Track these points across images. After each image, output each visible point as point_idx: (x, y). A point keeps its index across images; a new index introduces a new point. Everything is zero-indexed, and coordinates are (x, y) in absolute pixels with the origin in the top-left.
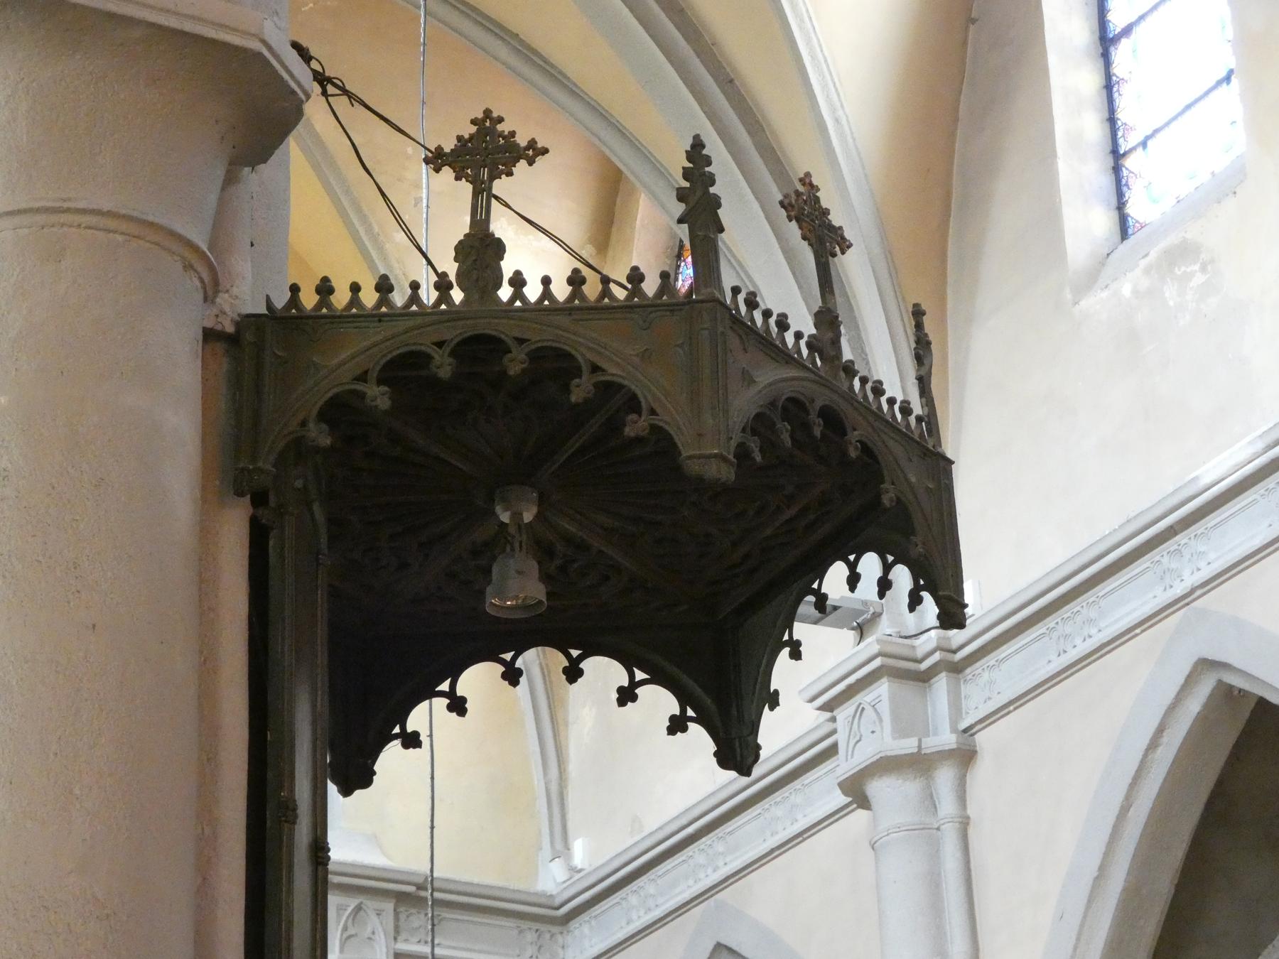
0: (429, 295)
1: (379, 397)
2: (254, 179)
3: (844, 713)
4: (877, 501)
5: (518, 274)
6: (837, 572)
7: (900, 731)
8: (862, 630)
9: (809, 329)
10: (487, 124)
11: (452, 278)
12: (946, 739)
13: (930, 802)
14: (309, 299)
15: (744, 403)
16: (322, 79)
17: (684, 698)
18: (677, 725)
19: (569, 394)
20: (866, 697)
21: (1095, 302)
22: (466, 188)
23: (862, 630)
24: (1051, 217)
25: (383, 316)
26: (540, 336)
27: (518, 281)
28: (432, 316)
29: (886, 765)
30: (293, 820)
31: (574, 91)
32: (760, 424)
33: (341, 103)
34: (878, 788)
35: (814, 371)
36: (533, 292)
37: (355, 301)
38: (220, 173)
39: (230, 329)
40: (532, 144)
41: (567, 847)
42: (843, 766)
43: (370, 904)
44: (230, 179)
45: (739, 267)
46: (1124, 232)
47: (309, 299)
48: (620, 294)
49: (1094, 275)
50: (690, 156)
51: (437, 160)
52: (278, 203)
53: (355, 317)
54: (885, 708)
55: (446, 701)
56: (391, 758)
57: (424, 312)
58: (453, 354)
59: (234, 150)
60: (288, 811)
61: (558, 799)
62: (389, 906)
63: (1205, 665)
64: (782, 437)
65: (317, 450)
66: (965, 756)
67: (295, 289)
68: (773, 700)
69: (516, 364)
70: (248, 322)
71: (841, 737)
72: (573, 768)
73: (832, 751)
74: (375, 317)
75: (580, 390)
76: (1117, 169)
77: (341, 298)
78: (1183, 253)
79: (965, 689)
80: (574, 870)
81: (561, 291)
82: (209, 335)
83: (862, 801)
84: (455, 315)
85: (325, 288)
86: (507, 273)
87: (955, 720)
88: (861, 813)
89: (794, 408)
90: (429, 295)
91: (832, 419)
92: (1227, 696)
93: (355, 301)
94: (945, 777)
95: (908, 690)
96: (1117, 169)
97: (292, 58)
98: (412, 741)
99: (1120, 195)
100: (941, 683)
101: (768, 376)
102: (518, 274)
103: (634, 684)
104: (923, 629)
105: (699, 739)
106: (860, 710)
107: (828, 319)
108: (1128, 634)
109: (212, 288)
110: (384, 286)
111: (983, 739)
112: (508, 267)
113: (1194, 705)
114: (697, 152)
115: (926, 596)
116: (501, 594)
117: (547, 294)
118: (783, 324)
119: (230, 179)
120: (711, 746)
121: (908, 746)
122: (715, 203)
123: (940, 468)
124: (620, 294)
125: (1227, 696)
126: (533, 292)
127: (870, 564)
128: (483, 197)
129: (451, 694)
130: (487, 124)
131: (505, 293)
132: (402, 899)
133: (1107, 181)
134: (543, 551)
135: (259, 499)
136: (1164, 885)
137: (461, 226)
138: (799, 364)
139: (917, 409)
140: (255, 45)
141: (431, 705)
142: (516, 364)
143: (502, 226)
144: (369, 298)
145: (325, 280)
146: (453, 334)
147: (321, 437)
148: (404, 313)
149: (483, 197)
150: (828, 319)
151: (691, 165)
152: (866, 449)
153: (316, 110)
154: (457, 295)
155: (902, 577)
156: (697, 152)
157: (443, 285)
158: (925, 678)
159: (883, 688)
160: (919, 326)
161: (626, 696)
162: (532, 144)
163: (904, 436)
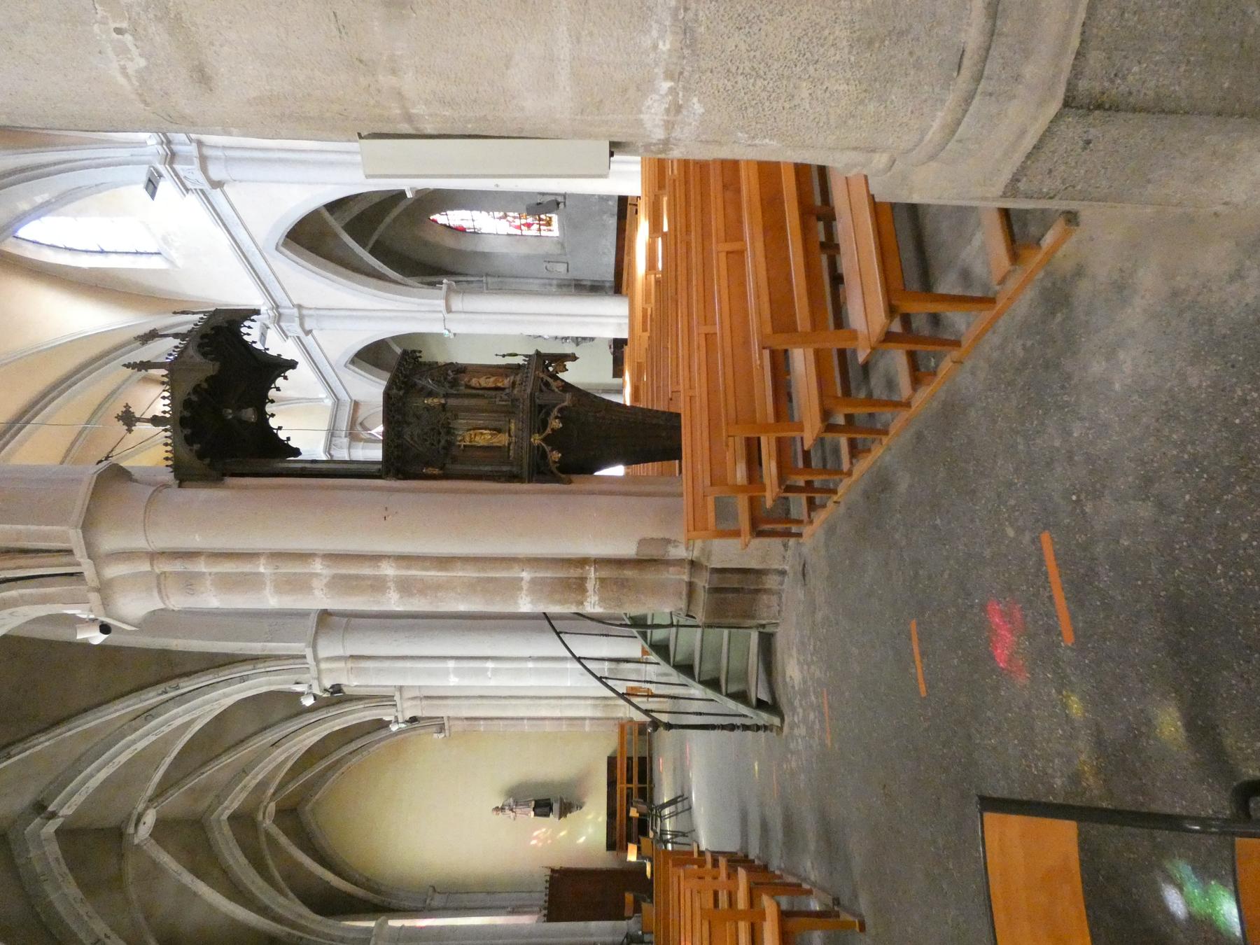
0: (168, 434)
1: (196, 447)
2: (136, 475)
3: (289, 334)
4: (227, 327)
6: (246, 338)
7: (293, 321)
8: (268, 328)
9: (179, 341)
10: (119, 418)
12: (295, 311)
13: (310, 316)
14: (170, 463)
15: (198, 358)
16: (107, 458)
17: (279, 376)
18: (286, 378)
19: (642, 125)
20: (285, 328)
21: (179, 263)
22: (137, 424)
23: (268, 328)
24: (154, 271)
25: (174, 445)
27: (164, 412)
28: (175, 432)
29: (302, 325)
30: (306, 468)
31: (118, 388)
32: (204, 355)
33: (114, 453)
34: (307, 327)
35: (190, 340)
36: (168, 409)
37: (170, 452)
38: (135, 484)
39: (178, 482)
40: (125, 407)
41: (321, 399)
42: (302, 335)
43: (333, 443)
44: (136, 481)
45: (158, 356)
46: (159, 253)
47: (170, 463)
48: (168, 387)
49: (172, 262)
50: (128, 368)
51: (130, 431)
52: (146, 469)
53: (174, 452)
54: (288, 324)
56: (292, 444)
60: (302, 469)
61: (310, 400)
62: (334, 439)
63: (277, 249)
65: (211, 461)
66: (300, 307)
67: (167, 466)
68: (279, 355)
69: (187, 414)
70: (176, 477)
71: (295, 335)
72: (302, 396)
73: (298, 338)
74: (174, 447)
75: (194, 398)
76: (142, 253)
77: (170, 455)
78: (165, 239)
79: (283, 305)
80: (327, 397)
81: (167, 402)
82: (180, 486)
83: (310, 332)
84: (173, 426)
85: (167, 459)
86: (163, 415)
87: (289, 308)
88: (314, 332)
89: (200, 346)
90: (168, 434)
91: (203, 337)
92: (285, 244)
93: (170, 452)
94: (305, 312)
95: (283, 318)
96: (142, 253)
97: (101, 465)
98: (288, 439)
99: (148, 253)
100: (281, 310)
101: (191, 351)
103: (275, 387)
105: (289, 373)
106: (288, 330)
107: (176, 336)
108: (269, 266)
109: (166, 486)
110: (166, 444)
111: (295, 303)
113: (288, 252)
114: (128, 366)
115: (252, 318)
116: (250, 418)
117: (168, 405)
118: (177, 347)
119: (136, 481)
120: (291, 370)
121: (297, 320)
122: (142, 362)
123: (217, 312)
124: (168, 387)
125: (285, 244)
126: (168, 409)
127: (244, 330)
128: (139, 420)
129: (277, 429)
130: (119, 418)
131: (168, 415)
132: (332, 435)
133: (144, 256)
134: (240, 408)
135: (224, 475)
136: (332, 265)
137: (149, 426)
138: (188, 344)
139: (202, 316)
140: (95, 476)
142: (187, 414)
143: (148, 415)
144: (169, 448)
146: (179, 429)
147: (207, 461)
148: (173, 440)
149: (139, 420)
150: (176, 336)
151: (431, 218)
152: (212, 329)
153: (113, 460)
154: (168, 427)
155: (247, 323)
156: (128, 366)
157: (166, 430)
158: (280, 314)
159: (282, 324)
160: (178, 313)
162: (125, 407)
163: (209, 319)
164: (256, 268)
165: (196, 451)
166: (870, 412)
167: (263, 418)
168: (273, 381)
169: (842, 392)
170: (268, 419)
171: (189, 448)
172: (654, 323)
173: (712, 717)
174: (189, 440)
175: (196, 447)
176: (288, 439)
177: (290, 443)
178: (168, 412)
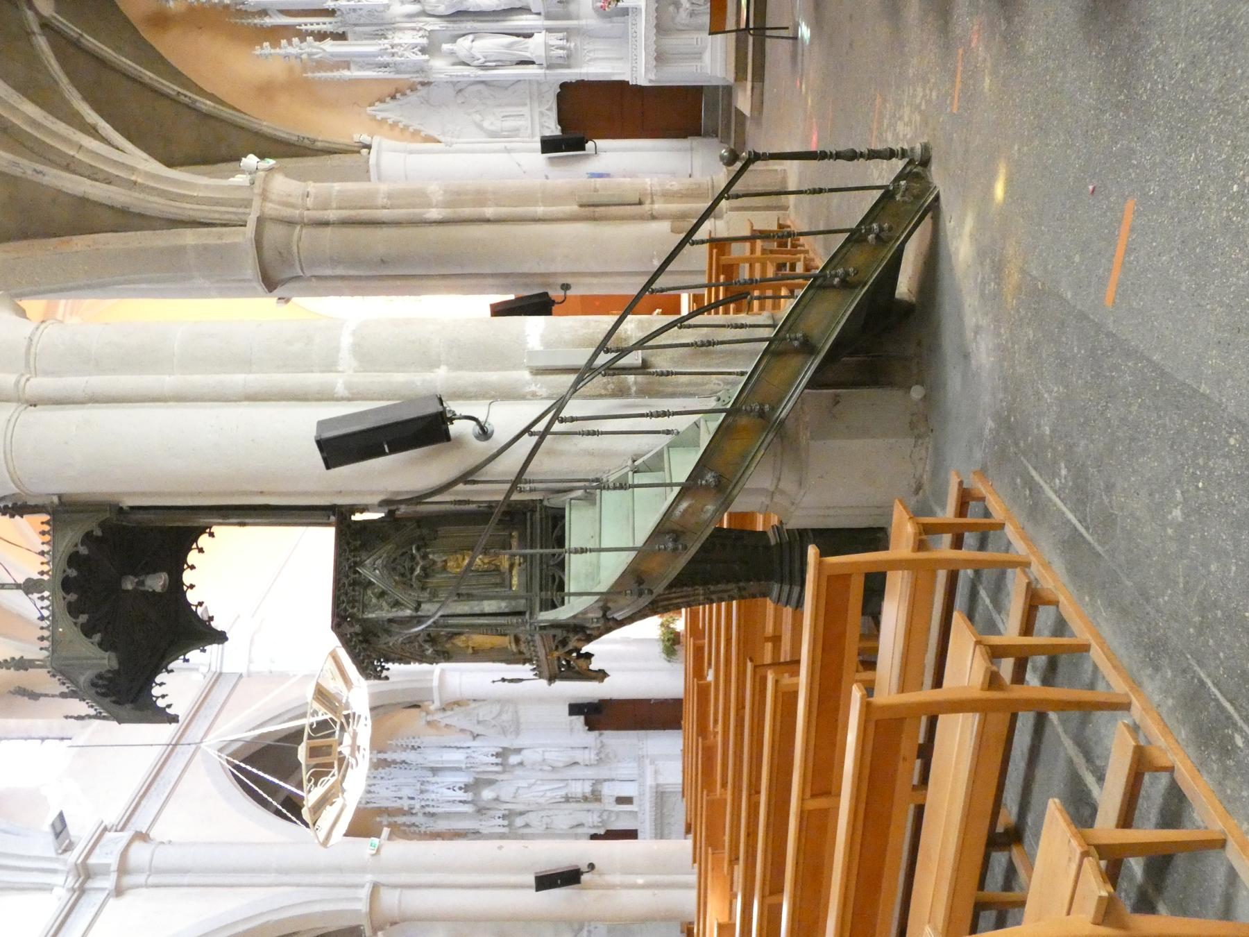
5: (39, 573)
11: (39, 595)
26: (64, 564)
27: (42, 573)
28: (54, 569)
36: (46, 568)
55: (199, 607)
57: (52, 604)
58: (82, 545)
59: (350, 35)
64: (266, 44)
77: (46, 633)
84: (53, 594)
85: (42, 639)
86: (39, 577)
102: (39, 573)
103: (188, 587)
104: (867, 184)
112: (36, 576)
129: (198, 548)
131: (46, 577)
141: (223, 649)
142: (73, 573)
145: (39, 639)
146: (61, 594)
154: (46, 594)
157: (42, 598)
161: (201, 550)
164: (137, 814)
165: (82, 625)
166: (1127, 831)
167: (177, 588)
168: (196, 540)
169: (1006, 193)
170: (184, 570)
171: (74, 620)
172: (769, 629)
173: (761, 198)
174: (73, 610)
175: (83, 618)
176: (204, 651)
177: (213, 624)
178: (47, 573)
